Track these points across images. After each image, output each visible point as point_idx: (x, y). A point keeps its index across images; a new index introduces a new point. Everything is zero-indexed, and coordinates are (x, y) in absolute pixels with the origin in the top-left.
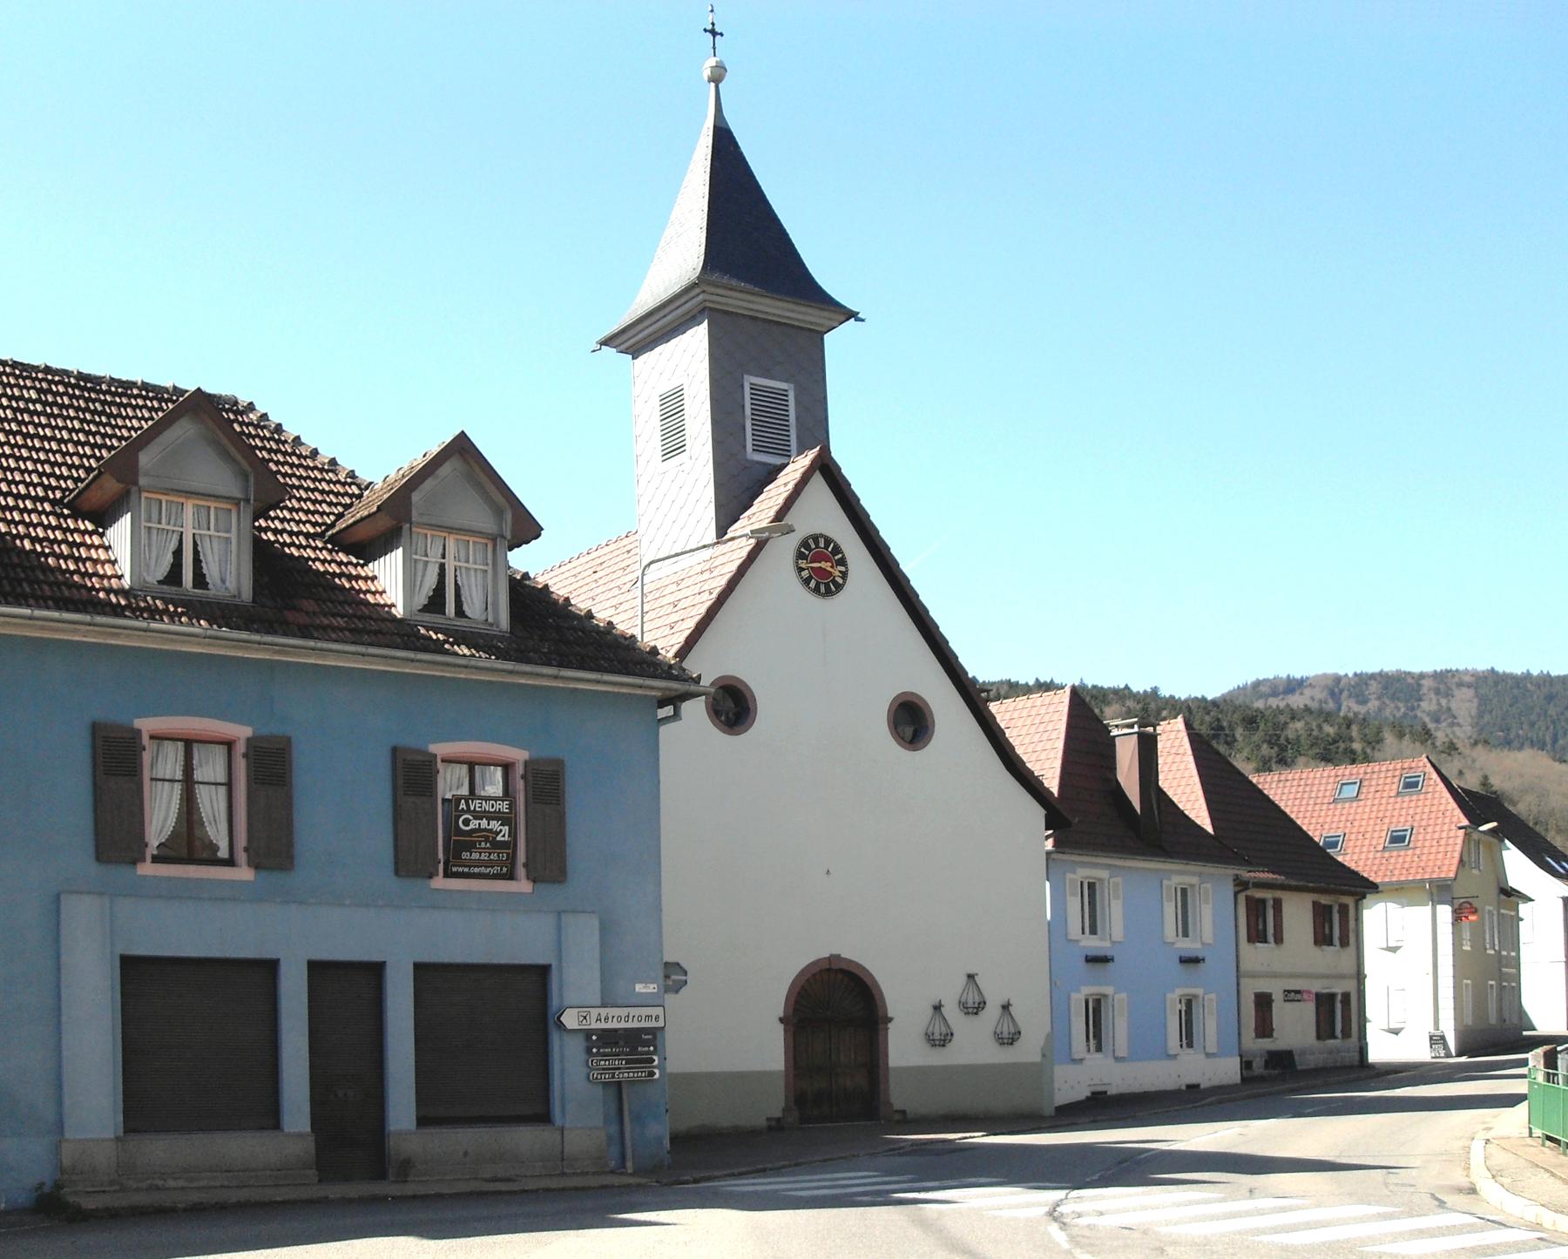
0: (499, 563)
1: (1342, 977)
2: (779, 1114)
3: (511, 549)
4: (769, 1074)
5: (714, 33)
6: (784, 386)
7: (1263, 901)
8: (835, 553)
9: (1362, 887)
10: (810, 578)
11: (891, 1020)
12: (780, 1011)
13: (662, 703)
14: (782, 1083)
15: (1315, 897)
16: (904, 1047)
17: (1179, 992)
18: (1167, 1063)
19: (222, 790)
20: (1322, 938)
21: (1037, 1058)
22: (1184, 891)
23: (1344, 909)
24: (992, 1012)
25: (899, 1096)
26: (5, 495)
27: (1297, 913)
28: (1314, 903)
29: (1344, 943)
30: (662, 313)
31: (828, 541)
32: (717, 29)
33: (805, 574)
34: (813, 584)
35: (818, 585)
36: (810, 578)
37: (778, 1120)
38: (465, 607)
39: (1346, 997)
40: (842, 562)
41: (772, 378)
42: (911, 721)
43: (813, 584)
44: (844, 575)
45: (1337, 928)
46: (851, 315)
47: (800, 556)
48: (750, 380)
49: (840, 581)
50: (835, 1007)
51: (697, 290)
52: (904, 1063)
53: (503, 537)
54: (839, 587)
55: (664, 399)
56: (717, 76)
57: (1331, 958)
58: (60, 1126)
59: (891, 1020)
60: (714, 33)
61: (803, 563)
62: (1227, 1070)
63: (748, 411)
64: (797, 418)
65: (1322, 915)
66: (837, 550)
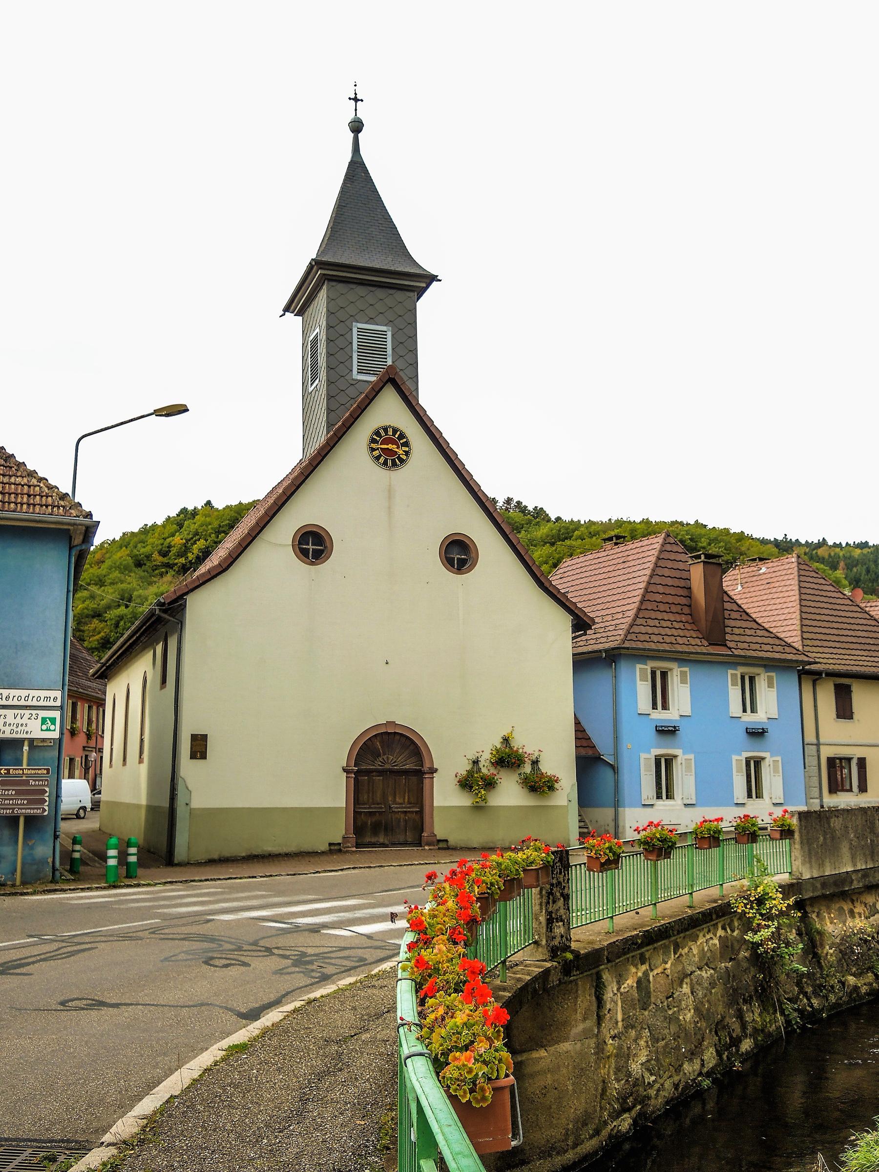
2: (339, 840)
4: (138, 806)
5: (356, 100)
6: (384, 328)
7: (736, 675)
8: (401, 438)
10: (380, 456)
14: (143, 813)
16: (445, 794)
19: (822, 740)
26: (4, 475)
28: (835, 685)
31: (395, 431)
32: (359, 97)
33: (376, 453)
35: (386, 460)
36: (380, 456)
40: (406, 444)
42: (458, 554)
44: (407, 453)
47: (373, 441)
48: (356, 326)
49: (404, 457)
56: (357, 127)
58: (809, 850)
60: (356, 100)
61: (374, 446)
66: (402, 436)
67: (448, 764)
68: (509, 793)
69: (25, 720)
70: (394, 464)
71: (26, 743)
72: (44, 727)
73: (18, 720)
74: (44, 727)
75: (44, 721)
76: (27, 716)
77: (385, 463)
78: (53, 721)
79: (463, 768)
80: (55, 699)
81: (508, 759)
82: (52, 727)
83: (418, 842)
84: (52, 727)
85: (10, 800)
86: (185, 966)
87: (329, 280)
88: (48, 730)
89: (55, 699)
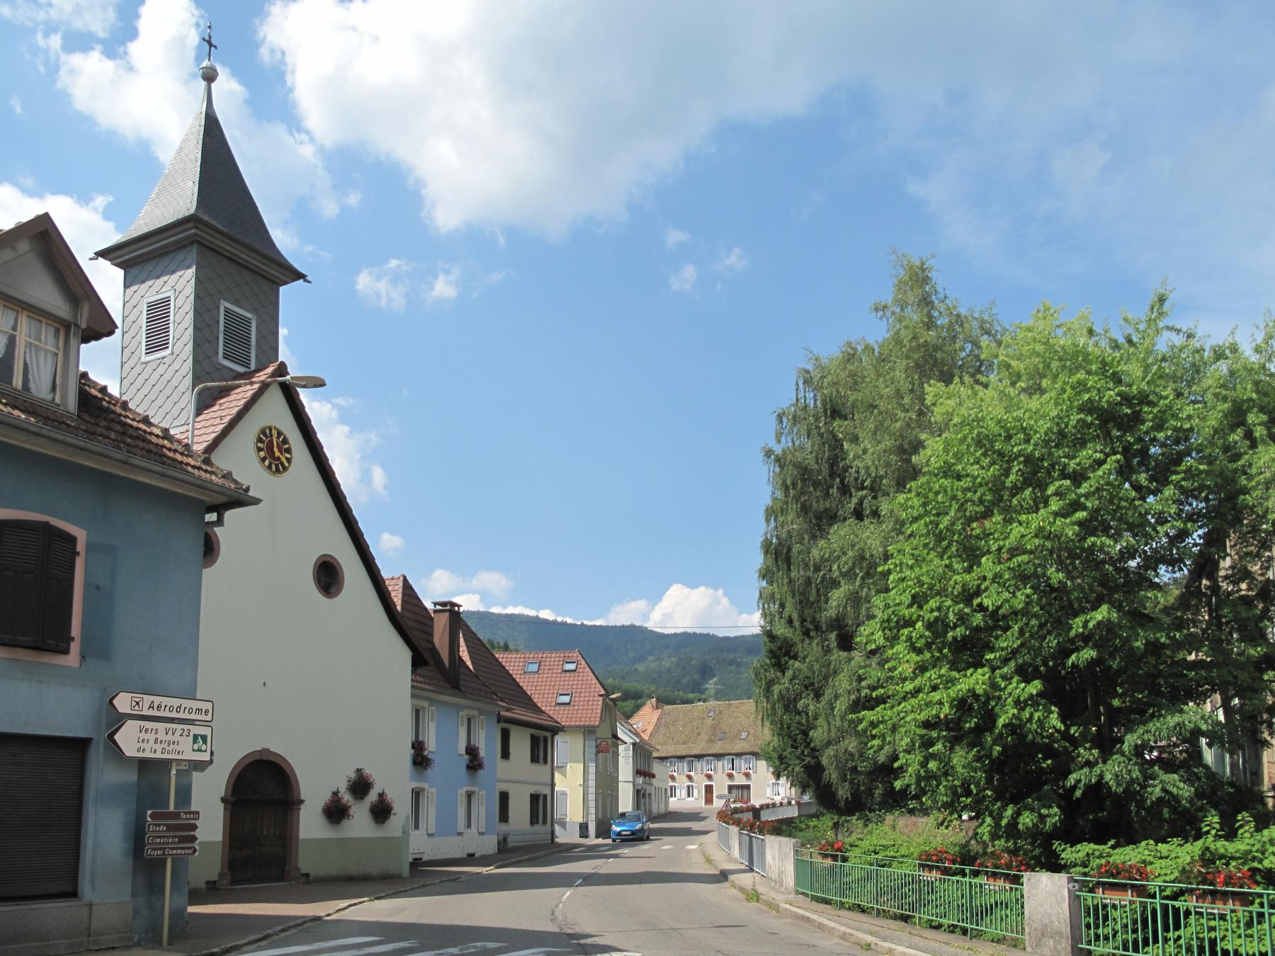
0: (69, 357)
1: (544, 784)
2: (214, 877)
3: (86, 340)
9: (556, 730)
11: (303, 801)
12: (222, 792)
13: (210, 509)
15: (534, 731)
16: (310, 824)
17: (466, 789)
18: (457, 838)
20: (534, 759)
21: (399, 834)
22: (469, 720)
23: (546, 739)
24: (372, 796)
25: (306, 862)
27: (521, 744)
29: (545, 762)
30: (156, 238)
34: (267, 463)
35: (270, 464)
37: (215, 882)
38: (32, 385)
39: (545, 796)
40: (289, 451)
41: (242, 307)
42: (328, 576)
43: (267, 463)
44: (289, 460)
45: (540, 751)
46: (301, 276)
48: (224, 304)
50: (263, 787)
51: (190, 225)
52: (309, 837)
53: (76, 325)
54: (285, 468)
55: (151, 306)
57: (540, 771)
59: (303, 801)
62: (489, 845)
63: (222, 328)
64: (257, 341)
65: (535, 741)
67: (314, 790)
68: (360, 815)
69: (176, 737)
70: (278, 471)
71: (174, 764)
72: (196, 747)
73: (170, 737)
74: (196, 747)
75: (195, 737)
76: (178, 732)
77: (269, 467)
78: (204, 738)
79: (326, 797)
80: (207, 711)
81: (360, 786)
82: (204, 747)
83: (281, 877)
84: (204, 747)
85: (161, 837)
86: (885, 847)
87: (201, 244)
88: (199, 750)
89: (207, 711)
